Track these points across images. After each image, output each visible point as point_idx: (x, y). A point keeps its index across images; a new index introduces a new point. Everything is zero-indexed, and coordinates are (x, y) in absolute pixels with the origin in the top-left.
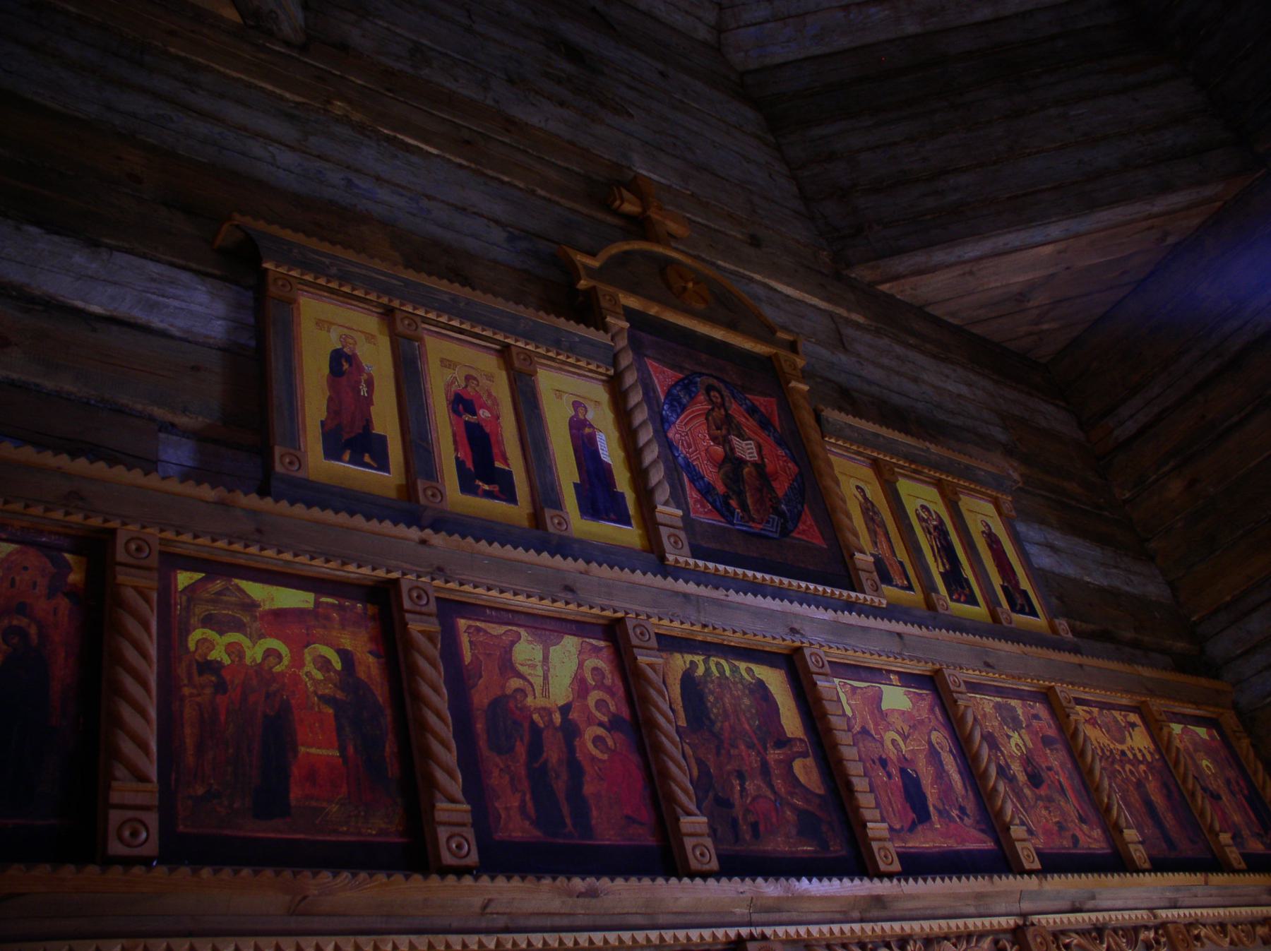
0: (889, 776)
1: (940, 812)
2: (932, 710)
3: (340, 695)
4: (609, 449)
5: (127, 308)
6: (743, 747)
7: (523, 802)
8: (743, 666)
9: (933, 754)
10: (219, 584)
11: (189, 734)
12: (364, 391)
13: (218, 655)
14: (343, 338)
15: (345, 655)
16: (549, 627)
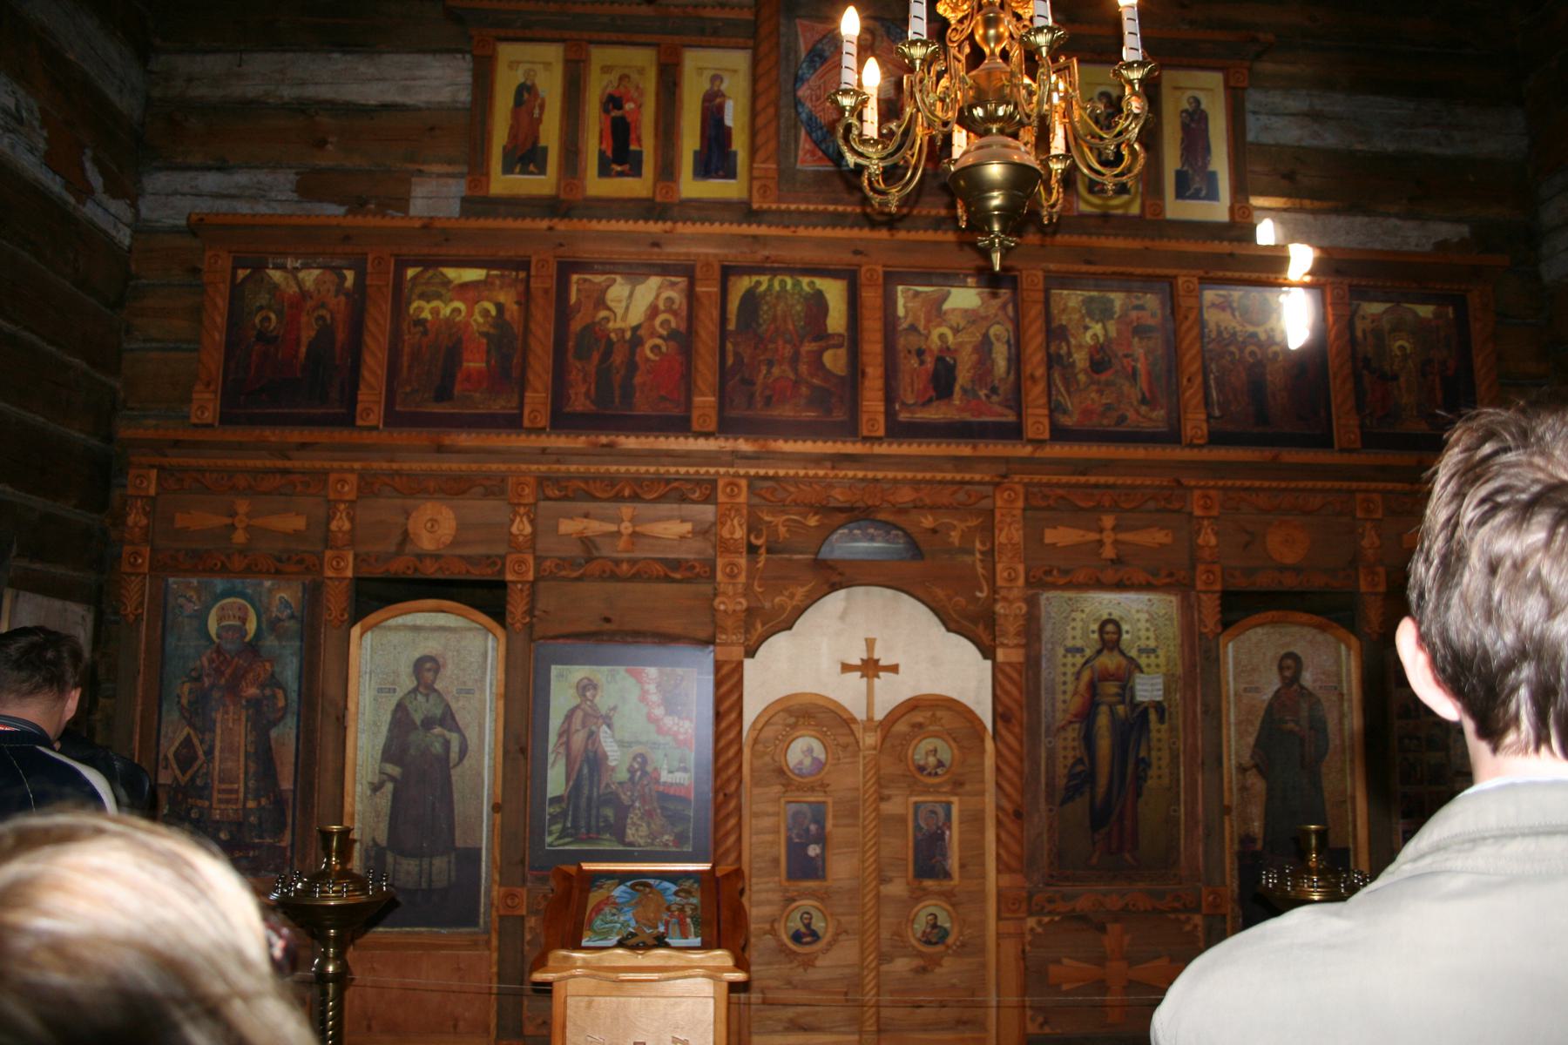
0: (922, 363)
1: (964, 391)
2: (1004, 307)
3: (492, 331)
4: (734, 115)
5: (393, 96)
6: (780, 342)
7: (589, 390)
8: (805, 281)
9: (984, 347)
10: (430, 273)
11: (405, 360)
12: (536, 112)
13: (426, 315)
14: (527, 73)
15: (500, 307)
16: (636, 271)
